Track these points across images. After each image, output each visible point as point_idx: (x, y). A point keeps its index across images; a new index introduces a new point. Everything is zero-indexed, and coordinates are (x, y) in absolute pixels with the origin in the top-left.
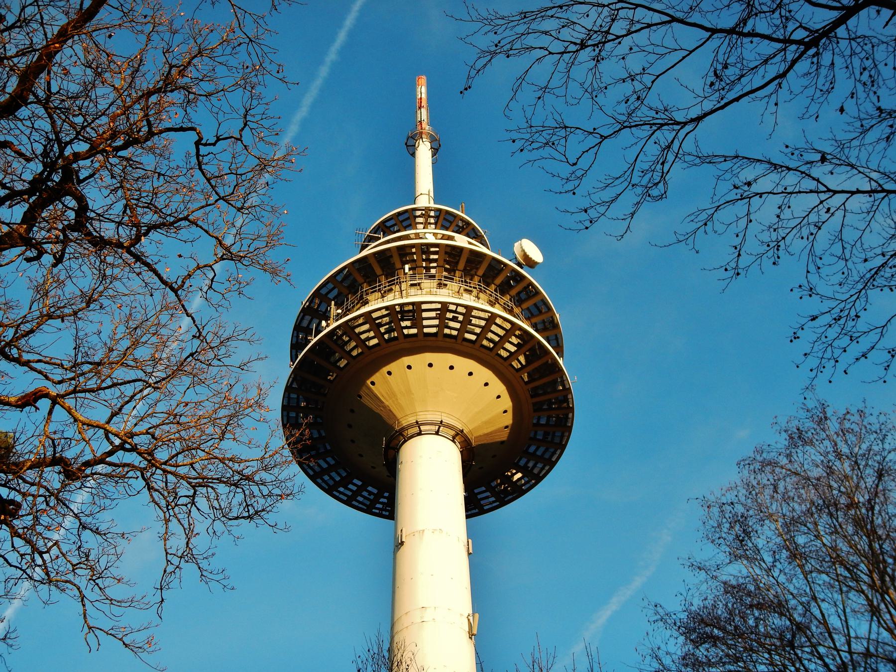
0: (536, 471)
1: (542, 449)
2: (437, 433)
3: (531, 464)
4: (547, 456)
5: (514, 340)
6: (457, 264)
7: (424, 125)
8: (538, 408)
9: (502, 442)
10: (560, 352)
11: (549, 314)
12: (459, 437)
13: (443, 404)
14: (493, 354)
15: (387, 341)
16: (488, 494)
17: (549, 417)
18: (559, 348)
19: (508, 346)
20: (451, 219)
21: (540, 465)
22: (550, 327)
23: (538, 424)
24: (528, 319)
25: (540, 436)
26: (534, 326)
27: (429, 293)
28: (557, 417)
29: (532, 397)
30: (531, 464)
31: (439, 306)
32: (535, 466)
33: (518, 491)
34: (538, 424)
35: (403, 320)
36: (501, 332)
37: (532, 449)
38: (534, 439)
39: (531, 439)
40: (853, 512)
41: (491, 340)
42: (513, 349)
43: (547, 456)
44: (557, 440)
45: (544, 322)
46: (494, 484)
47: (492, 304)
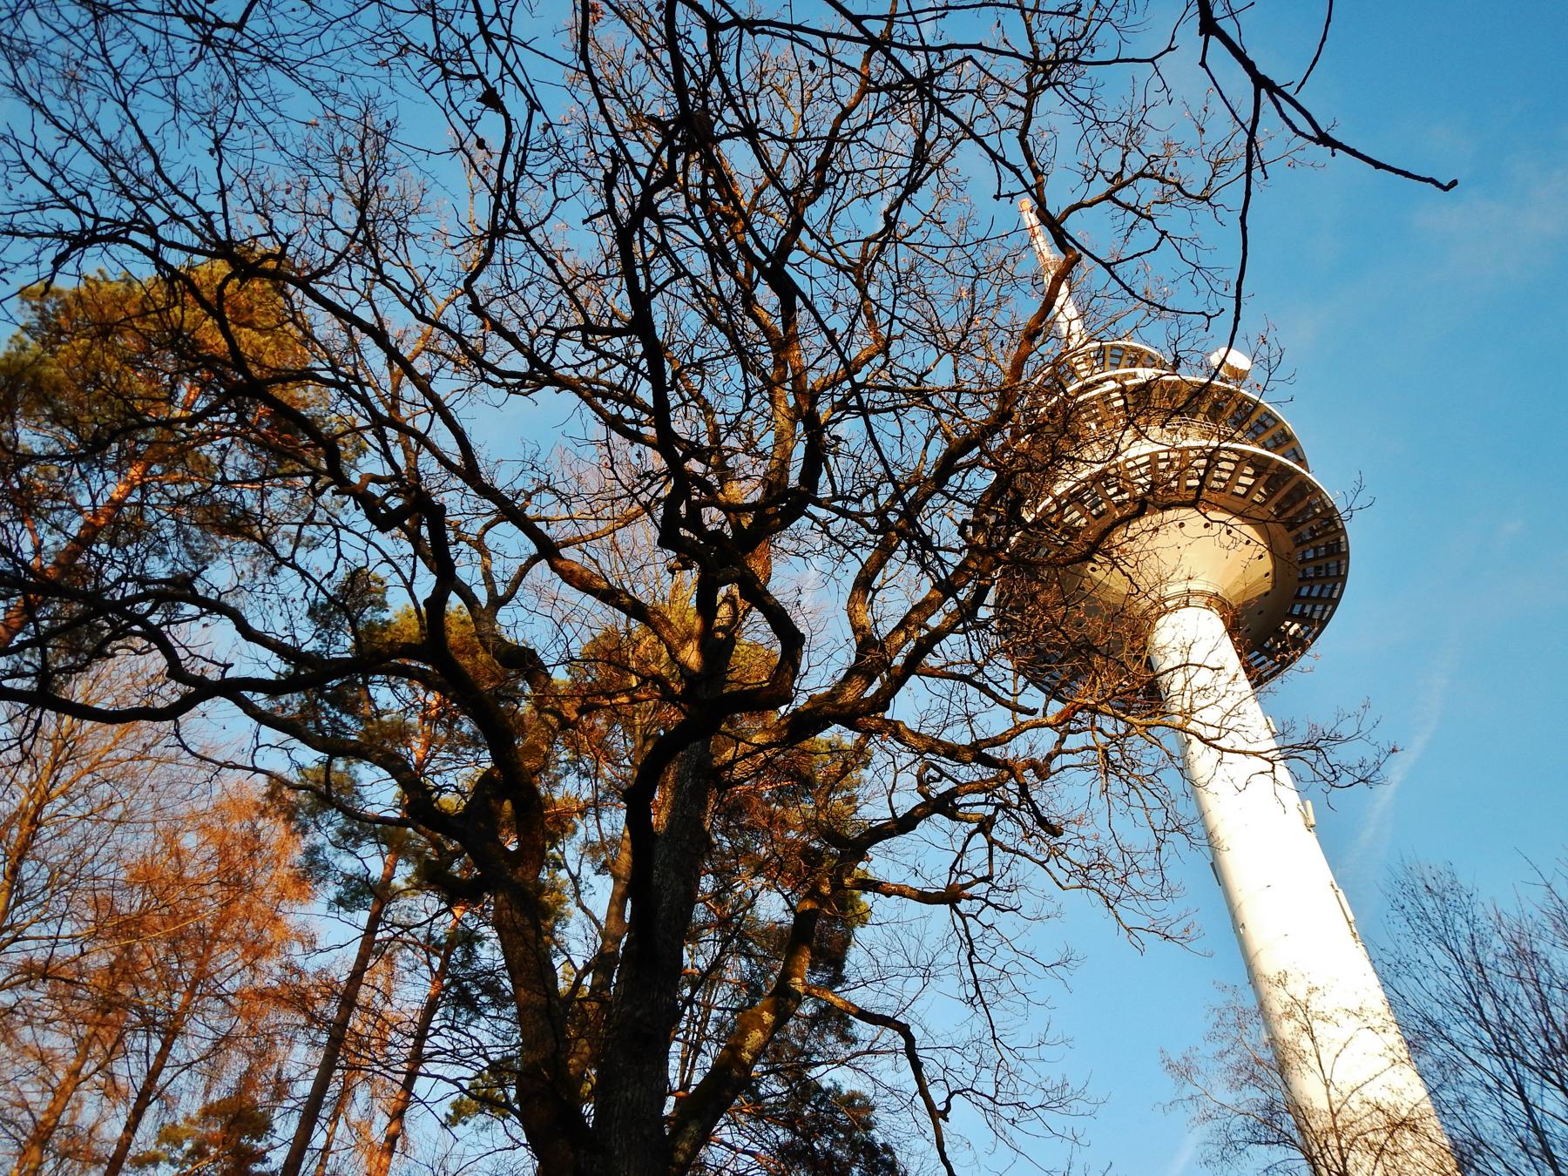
0: (1316, 616)
1: (1317, 589)
2: (1187, 605)
3: (1308, 610)
4: (1325, 594)
5: (1249, 471)
6: (1141, 404)
7: (1046, 255)
8: (1300, 542)
9: (1267, 594)
10: (1305, 466)
11: (1278, 427)
12: (1217, 602)
13: (1196, 563)
14: (1227, 494)
15: (1096, 517)
16: (1264, 658)
17: (1316, 549)
18: (1301, 461)
19: (1243, 480)
20: (1119, 353)
21: (1319, 608)
22: (1284, 440)
23: (1304, 561)
24: (1254, 441)
25: (1311, 572)
26: (1264, 446)
27: (1140, 449)
28: (1327, 545)
29: (1289, 530)
30: (1308, 610)
31: (1146, 459)
32: (1313, 610)
33: (1301, 644)
34: (1304, 561)
35: (1108, 487)
36: (1231, 466)
37: (1304, 592)
38: (1304, 579)
39: (1300, 580)
40: (808, 805)
41: (1220, 480)
42: (1250, 481)
43: (1325, 594)
44: (1333, 573)
45: (1274, 438)
46: (1267, 645)
47: (1208, 436)
